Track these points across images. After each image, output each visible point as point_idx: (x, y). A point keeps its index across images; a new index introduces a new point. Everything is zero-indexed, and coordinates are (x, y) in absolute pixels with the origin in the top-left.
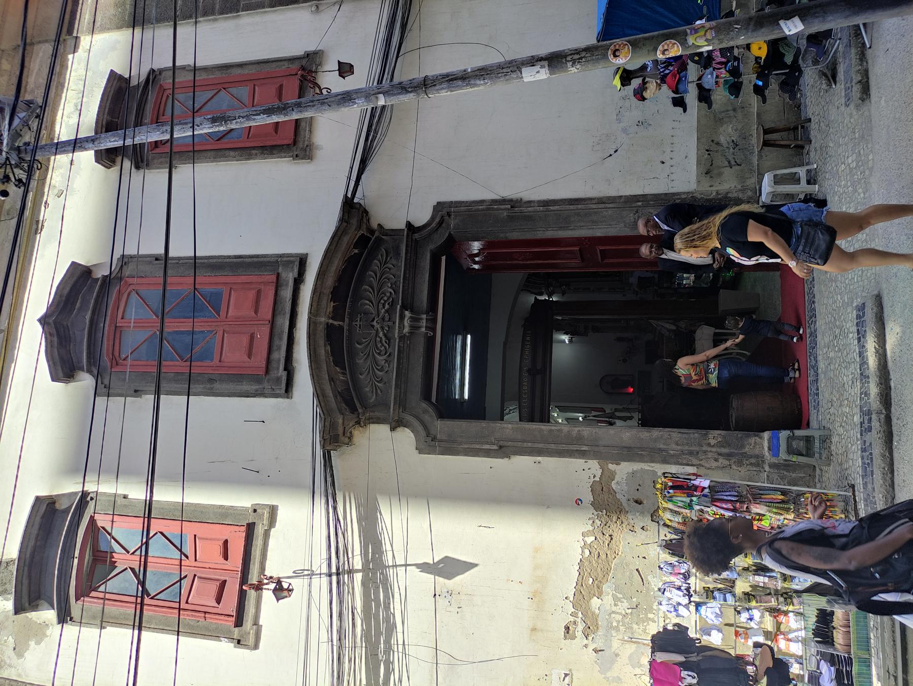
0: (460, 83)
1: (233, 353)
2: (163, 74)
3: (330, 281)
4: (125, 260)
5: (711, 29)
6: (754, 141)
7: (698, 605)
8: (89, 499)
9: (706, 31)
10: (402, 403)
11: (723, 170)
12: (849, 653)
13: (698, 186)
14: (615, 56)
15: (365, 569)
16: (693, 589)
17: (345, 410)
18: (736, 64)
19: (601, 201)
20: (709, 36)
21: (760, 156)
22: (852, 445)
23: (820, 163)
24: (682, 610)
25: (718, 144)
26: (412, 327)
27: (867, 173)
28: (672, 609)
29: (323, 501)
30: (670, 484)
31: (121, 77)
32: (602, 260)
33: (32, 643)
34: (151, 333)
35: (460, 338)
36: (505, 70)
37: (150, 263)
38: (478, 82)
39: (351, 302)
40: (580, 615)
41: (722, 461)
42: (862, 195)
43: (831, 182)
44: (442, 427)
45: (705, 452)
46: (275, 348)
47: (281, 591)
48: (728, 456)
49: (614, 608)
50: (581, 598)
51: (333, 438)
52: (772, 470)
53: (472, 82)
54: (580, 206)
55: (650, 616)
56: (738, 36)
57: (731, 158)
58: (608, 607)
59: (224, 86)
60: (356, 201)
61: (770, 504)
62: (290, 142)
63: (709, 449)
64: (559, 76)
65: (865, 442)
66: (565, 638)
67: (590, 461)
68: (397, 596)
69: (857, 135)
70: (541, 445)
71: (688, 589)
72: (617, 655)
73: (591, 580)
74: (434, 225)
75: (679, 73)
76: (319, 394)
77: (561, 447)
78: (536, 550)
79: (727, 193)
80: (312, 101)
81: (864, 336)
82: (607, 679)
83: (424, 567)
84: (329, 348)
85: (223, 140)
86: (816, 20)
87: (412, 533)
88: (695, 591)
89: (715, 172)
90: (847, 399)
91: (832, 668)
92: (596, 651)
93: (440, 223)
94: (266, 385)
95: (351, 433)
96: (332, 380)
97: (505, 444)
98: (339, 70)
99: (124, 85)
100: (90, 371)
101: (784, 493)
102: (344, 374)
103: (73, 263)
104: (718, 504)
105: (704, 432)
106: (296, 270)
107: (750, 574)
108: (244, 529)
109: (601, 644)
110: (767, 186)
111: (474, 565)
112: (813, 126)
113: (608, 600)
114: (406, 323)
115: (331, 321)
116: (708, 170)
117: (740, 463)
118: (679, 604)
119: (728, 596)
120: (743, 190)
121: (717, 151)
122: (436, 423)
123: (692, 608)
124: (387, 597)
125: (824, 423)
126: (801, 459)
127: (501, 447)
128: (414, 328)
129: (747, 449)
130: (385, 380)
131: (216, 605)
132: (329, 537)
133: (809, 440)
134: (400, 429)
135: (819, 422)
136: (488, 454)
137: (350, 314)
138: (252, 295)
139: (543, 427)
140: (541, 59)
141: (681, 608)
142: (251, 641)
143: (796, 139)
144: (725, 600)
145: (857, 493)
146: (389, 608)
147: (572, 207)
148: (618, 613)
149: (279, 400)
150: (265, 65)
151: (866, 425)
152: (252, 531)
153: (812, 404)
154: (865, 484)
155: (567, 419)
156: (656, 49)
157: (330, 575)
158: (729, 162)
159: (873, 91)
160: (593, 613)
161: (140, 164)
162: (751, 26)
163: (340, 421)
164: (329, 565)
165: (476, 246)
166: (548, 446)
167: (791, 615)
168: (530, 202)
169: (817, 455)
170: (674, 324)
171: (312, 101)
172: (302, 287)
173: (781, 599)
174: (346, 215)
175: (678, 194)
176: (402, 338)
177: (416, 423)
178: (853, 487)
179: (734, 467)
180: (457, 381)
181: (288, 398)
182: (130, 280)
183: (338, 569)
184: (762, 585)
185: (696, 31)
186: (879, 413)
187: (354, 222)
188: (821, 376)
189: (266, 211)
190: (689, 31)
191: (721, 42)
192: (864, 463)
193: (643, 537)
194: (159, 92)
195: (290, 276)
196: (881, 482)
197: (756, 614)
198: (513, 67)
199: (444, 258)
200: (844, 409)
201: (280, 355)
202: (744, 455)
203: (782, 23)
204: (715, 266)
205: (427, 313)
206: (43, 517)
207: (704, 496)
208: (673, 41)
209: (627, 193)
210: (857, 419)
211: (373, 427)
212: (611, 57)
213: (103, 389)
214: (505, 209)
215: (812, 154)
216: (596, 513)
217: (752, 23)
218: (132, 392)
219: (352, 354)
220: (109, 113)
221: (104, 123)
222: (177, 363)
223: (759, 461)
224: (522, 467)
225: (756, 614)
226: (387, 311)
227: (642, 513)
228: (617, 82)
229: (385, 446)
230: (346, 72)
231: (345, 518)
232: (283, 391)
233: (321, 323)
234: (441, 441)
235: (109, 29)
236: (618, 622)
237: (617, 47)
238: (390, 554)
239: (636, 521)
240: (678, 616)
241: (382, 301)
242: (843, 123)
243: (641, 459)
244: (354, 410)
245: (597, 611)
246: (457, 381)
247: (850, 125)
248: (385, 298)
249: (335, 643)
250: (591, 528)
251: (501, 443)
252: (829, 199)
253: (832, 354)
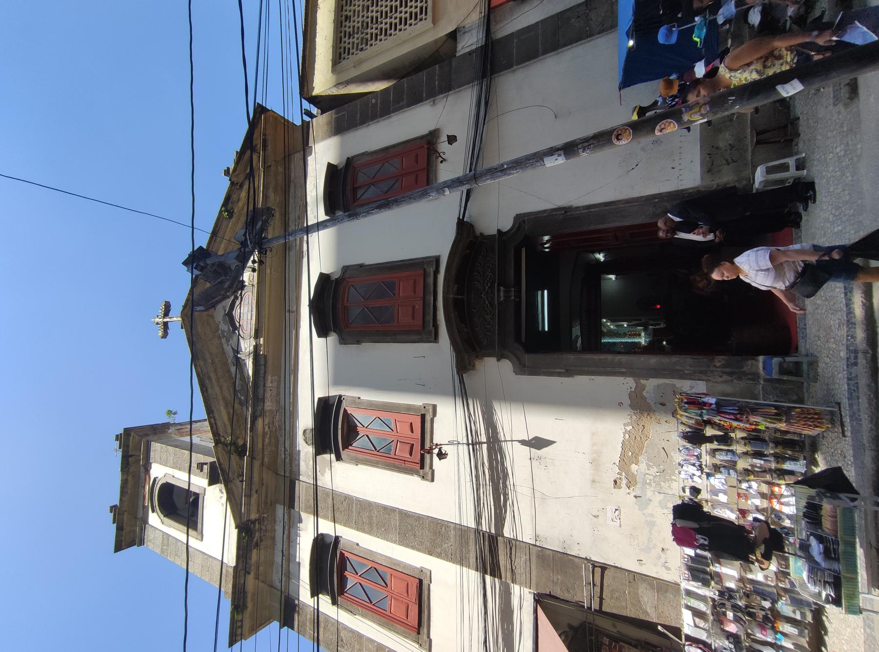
12: (836, 537)
15: (488, 442)
16: (704, 463)
17: (469, 350)
20: (703, 112)
21: (753, 153)
25: (717, 148)
26: (505, 297)
27: (855, 159)
35: (540, 292)
41: (725, 377)
42: (850, 178)
44: (528, 358)
45: (712, 371)
48: (730, 374)
49: (647, 472)
50: (624, 463)
51: (464, 365)
61: (765, 416)
64: (573, 161)
65: (851, 373)
68: (508, 458)
69: (845, 129)
71: (700, 466)
76: (453, 342)
78: (593, 434)
81: (851, 292)
82: (644, 514)
83: (523, 442)
87: (515, 422)
88: (706, 466)
91: (821, 546)
92: (636, 497)
100: (335, 331)
101: (776, 407)
110: (760, 176)
113: (643, 466)
114: (502, 294)
118: (694, 475)
123: (704, 476)
124: (502, 458)
128: (507, 297)
133: (798, 364)
134: (503, 360)
136: (559, 375)
144: (729, 474)
145: (842, 409)
151: (852, 360)
153: (800, 335)
154: (851, 405)
155: (617, 326)
157: (468, 444)
158: (727, 161)
159: (862, 91)
160: (633, 474)
165: (546, 238)
173: (775, 475)
176: (500, 303)
178: (839, 404)
180: (540, 316)
185: (690, 108)
186: (865, 352)
189: (418, 231)
190: (684, 109)
192: (849, 389)
195: (431, 270)
196: (867, 405)
198: (538, 158)
199: (524, 250)
200: (831, 345)
203: (779, 88)
208: (669, 120)
210: (843, 354)
211: (486, 359)
212: (615, 141)
215: (801, 145)
223: (755, 377)
224: (582, 382)
227: (666, 412)
229: (495, 369)
235: (324, 139)
240: (693, 481)
243: (664, 376)
246: (540, 316)
247: (838, 121)
252: (816, 181)
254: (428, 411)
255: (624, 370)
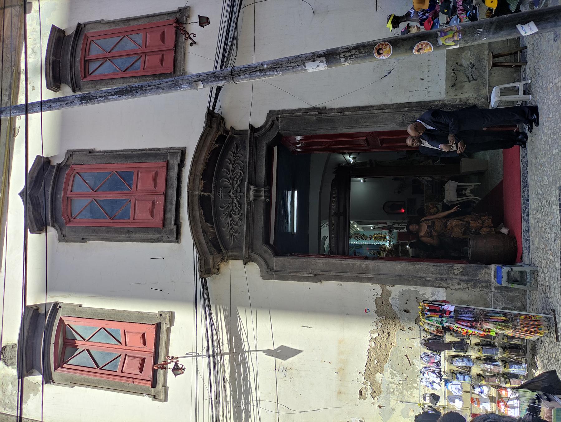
0: (259, 73)
1: (142, 214)
2: (87, 26)
3: (200, 167)
4: (71, 154)
5: (458, 32)
6: (486, 62)
7: (447, 382)
8: (58, 307)
9: (454, 34)
10: (251, 246)
11: (463, 84)
13: (446, 95)
14: (379, 54)
15: (231, 353)
17: (214, 252)
18: (474, 12)
19: (380, 107)
20: (456, 38)
21: (490, 73)
22: (554, 283)
23: (533, 79)
24: (435, 386)
25: (461, 65)
28: (429, 385)
29: (203, 311)
30: (428, 308)
31: (59, 30)
32: (382, 145)
33: (31, 395)
34: (89, 201)
35: (290, 192)
36: (292, 64)
37: (86, 155)
38: (272, 73)
39: (215, 180)
40: (369, 384)
41: (463, 285)
43: (541, 95)
44: (277, 262)
45: (451, 279)
46: (168, 210)
47: (177, 370)
48: (467, 281)
49: (391, 380)
50: (369, 373)
51: (207, 270)
52: (496, 291)
53: (268, 73)
54: (365, 112)
55: (415, 385)
56: (480, 38)
57: (469, 75)
58: (387, 379)
59: (126, 34)
60: (216, 111)
61: (496, 322)
62: (171, 71)
63: (454, 277)
64: (334, 69)
66: (360, 398)
67: (374, 285)
68: (251, 370)
70: (341, 274)
71: (439, 373)
72: (393, 410)
73: (376, 362)
74: (267, 127)
75: (433, 20)
76: (197, 243)
77: (355, 275)
78: (340, 342)
79: (467, 100)
80: (150, 86)
83: (269, 352)
84: (202, 211)
85: (127, 71)
86: (549, 25)
87: (260, 331)
89: (459, 85)
90: (550, 250)
93: (272, 125)
94: (164, 235)
95: (219, 266)
96: (204, 232)
97: (318, 273)
98: (200, 22)
99: (62, 35)
100: (53, 226)
101: (505, 315)
102: (213, 227)
103: (38, 156)
104: (461, 323)
105: (450, 265)
106: (179, 159)
107: (481, 362)
108: (154, 326)
109: (383, 403)
111: (301, 351)
112: (529, 51)
113: (387, 375)
114: (252, 193)
115: (202, 193)
116: (454, 84)
117: (475, 286)
118: (434, 382)
119: (467, 377)
120: (478, 98)
121: (460, 71)
122: (273, 259)
123: (443, 383)
124: (245, 370)
125: (533, 261)
126: (517, 286)
127: (315, 275)
128: (257, 197)
129: (480, 277)
130: (239, 231)
131: (140, 374)
132: (208, 335)
135: (529, 260)
136: (307, 279)
137: (214, 188)
138: (151, 175)
139: (343, 262)
140: (320, 56)
141: (434, 384)
142: (162, 396)
143: (516, 61)
144: (464, 380)
146: (247, 377)
147: (360, 112)
148: (393, 383)
149: (172, 244)
150: (153, 19)
152: (160, 328)
153: (524, 246)
155: (363, 228)
156: (412, 48)
158: (468, 78)
160: (378, 383)
161: (76, 89)
162: (492, 30)
163: (211, 259)
164: (208, 350)
165: (299, 138)
166: (346, 274)
167: (509, 390)
168: (332, 109)
169: (528, 284)
170: (430, 177)
171: (150, 86)
172: (183, 169)
173: (502, 379)
174: (209, 122)
175: (433, 101)
176: (249, 203)
177: (260, 259)
178: (554, 311)
179: (471, 288)
181: (178, 243)
182: (75, 167)
183: (213, 353)
184: (489, 370)
187: (215, 126)
188: (532, 229)
191: (467, 43)
193: (410, 334)
194: (84, 39)
195: (175, 163)
197: (485, 389)
198: (298, 62)
199: (276, 148)
200: (548, 257)
201: (171, 215)
202: (478, 281)
203: (519, 27)
204: (457, 152)
205: (265, 187)
206: (31, 319)
207: (451, 317)
208: (426, 42)
209: (398, 102)
211: (233, 262)
213: (63, 238)
214: (315, 115)
215: (528, 72)
216: (378, 318)
217: (493, 27)
218: (81, 239)
219: (217, 215)
220: (53, 55)
221: (51, 62)
222: (107, 221)
225: (485, 389)
226: (239, 186)
227: (409, 319)
228: (390, 25)
229: (241, 274)
230: (204, 23)
231: (217, 321)
232: (175, 238)
233: (196, 195)
234: (276, 271)
236: (394, 389)
237: (381, 47)
238: (246, 344)
239: (405, 323)
241: (235, 179)
242: (552, 53)
243: (408, 283)
244: (220, 251)
245: (380, 382)
248: (238, 177)
249: (213, 399)
250: (376, 328)
251: (316, 273)
252: (539, 106)
253: (540, 216)
254: (165, 319)
255: (371, 276)
